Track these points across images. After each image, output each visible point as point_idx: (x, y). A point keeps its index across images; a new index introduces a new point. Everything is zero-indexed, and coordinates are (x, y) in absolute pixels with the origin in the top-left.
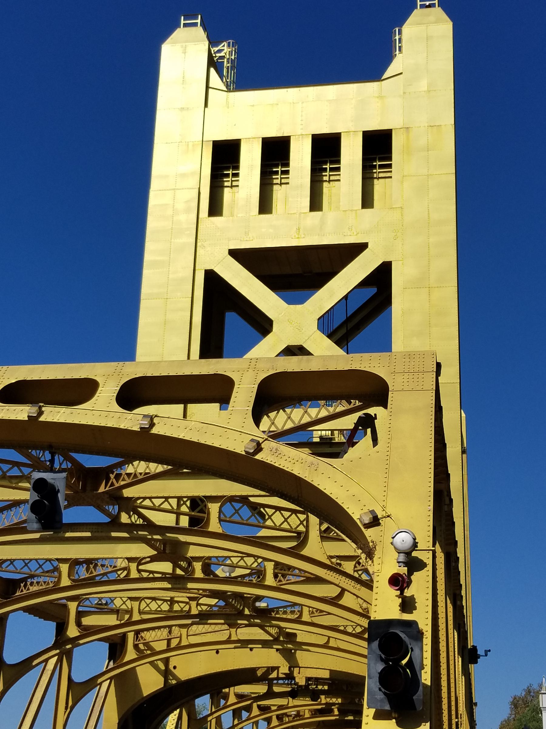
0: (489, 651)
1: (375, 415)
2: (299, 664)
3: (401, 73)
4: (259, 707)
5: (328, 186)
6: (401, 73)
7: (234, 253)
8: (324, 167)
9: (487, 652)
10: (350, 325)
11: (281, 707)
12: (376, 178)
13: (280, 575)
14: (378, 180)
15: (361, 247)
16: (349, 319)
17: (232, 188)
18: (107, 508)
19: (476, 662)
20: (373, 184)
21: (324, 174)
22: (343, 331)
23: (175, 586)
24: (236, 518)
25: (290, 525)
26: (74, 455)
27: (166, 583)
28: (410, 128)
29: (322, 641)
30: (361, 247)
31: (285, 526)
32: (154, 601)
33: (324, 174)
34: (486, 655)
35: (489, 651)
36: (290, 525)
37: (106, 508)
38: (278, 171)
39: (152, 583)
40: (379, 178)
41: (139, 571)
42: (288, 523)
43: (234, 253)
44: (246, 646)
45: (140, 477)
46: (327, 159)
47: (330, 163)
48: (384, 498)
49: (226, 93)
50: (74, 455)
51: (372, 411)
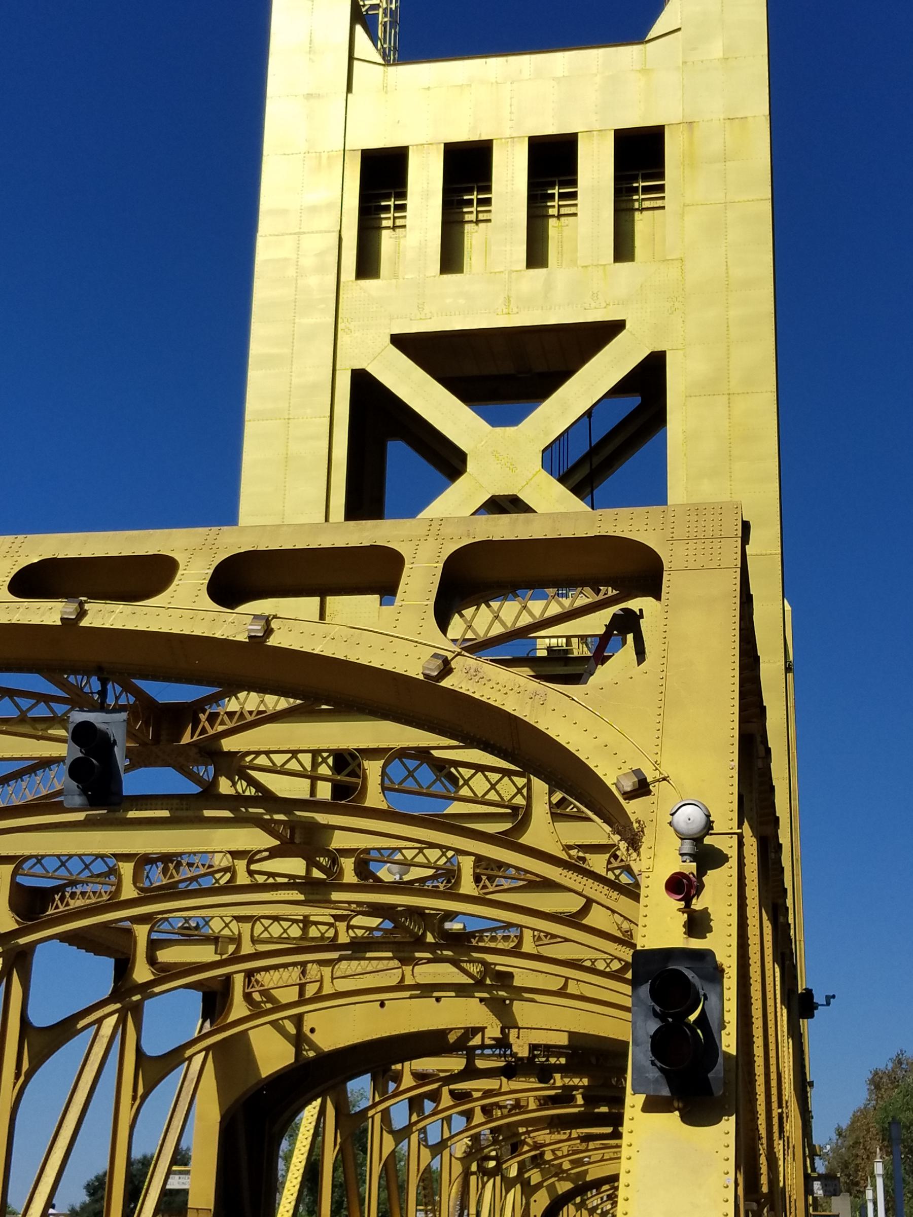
0: (834, 997)
1: (641, 610)
2: (517, 1023)
3: (679, 29)
4: (452, 1092)
5: (557, 225)
6: (679, 29)
7: (401, 342)
8: (550, 192)
9: (829, 999)
10: (596, 461)
11: (488, 1093)
12: (638, 210)
13: (484, 878)
14: (641, 213)
15: (616, 327)
16: (594, 451)
17: (394, 230)
18: (195, 769)
19: (812, 1016)
20: (633, 221)
21: (549, 204)
22: (585, 471)
23: (311, 897)
24: (410, 784)
25: (499, 795)
26: (141, 684)
27: (297, 892)
28: (694, 122)
29: (555, 984)
30: (616, 327)
31: (492, 796)
32: (276, 923)
33: (549, 204)
34: (828, 1004)
35: (834, 997)
36: (499, 795)
37: (69, 679)
38: (472, 200)
39: (272, 893)
40: (642, 210)
41: (251, 873)
42: (497, 792)
43: (401, 342)
44: (429, 994)
45: (250, 718)
46: (470, 185)
47: (395, 198)
48: (657, 749)
49: (382, 67)
50: (141, 684)
51: (634, 604)
